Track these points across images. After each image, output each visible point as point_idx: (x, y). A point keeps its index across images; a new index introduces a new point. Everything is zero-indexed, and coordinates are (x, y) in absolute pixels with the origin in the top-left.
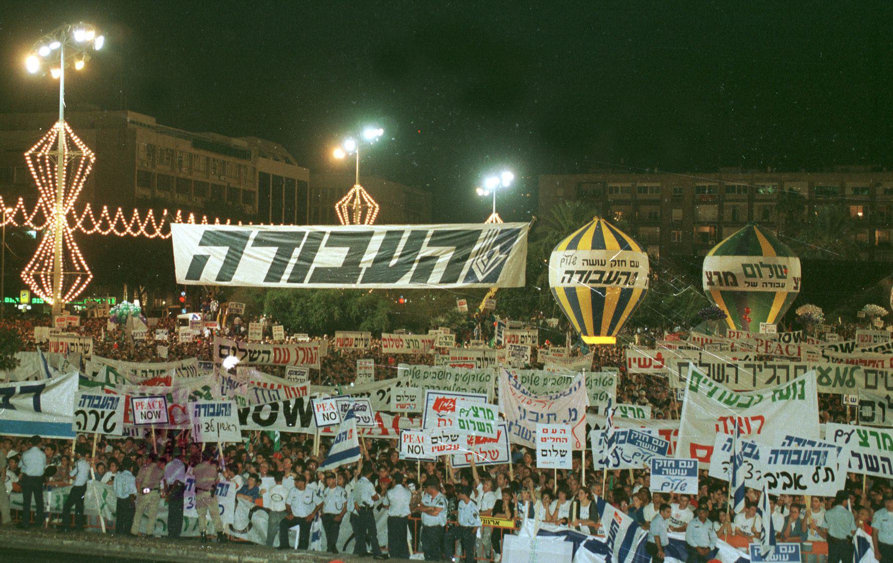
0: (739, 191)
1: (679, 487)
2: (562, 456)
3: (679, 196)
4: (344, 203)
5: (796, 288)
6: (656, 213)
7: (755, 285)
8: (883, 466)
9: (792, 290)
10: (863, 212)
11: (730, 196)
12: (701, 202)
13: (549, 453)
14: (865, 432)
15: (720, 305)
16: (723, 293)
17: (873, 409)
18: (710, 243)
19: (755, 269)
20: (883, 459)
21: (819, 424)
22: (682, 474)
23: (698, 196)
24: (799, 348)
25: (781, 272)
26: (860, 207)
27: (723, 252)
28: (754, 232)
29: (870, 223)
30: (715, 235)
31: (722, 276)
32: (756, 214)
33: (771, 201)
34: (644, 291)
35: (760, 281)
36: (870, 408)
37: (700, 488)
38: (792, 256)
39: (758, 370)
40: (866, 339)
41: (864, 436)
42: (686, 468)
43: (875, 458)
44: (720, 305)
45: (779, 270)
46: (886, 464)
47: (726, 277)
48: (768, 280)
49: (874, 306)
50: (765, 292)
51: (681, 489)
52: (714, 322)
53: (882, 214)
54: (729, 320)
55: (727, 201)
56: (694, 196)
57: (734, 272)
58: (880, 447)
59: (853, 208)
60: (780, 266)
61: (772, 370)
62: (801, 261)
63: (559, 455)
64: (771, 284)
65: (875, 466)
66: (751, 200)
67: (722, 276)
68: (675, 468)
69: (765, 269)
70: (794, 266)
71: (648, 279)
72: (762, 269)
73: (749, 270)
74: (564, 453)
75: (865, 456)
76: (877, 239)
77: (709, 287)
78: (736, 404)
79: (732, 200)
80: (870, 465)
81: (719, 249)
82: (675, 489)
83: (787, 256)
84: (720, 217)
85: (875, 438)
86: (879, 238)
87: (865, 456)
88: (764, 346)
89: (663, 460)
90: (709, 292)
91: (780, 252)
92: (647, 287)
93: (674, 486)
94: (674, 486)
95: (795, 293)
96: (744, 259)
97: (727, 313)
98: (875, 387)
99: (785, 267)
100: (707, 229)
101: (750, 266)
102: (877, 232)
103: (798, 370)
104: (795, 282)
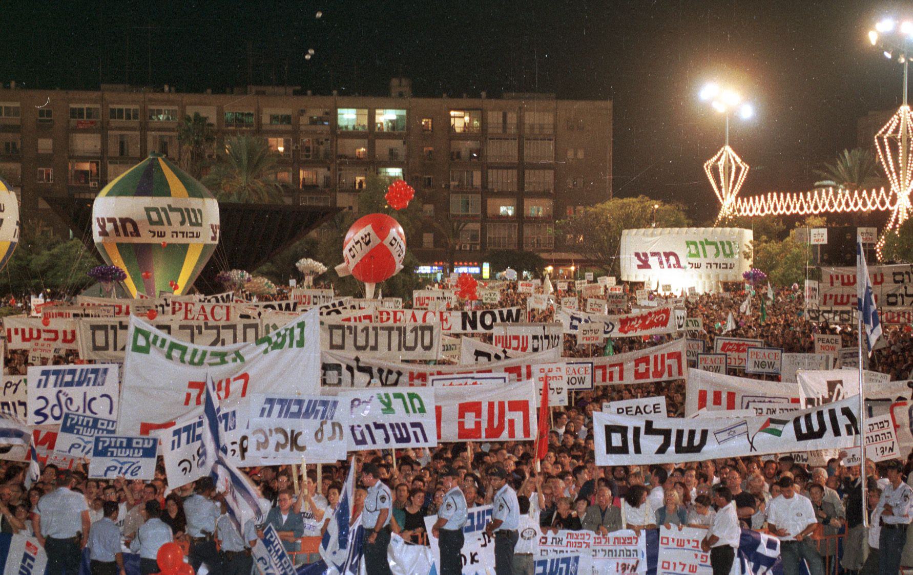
0: (129, 117)
1: (130, 471)
2: (558, 393)
3: (47, 121)
4: (719, 159)
5: (213, 239)
6: (14, 145)
7: (162, 235)
8: (415, 433)
9: (209, 241)
10: (284, 147)
11: (114, 122)
12: (76, 130)
13: (900, 299)
14: (387, 396)
15: (118, 262)
16: (120, 246)
17: (340, 374)
18: (91, 184)
19: (163, 214)
20: (414, 425)
21: (321, 388)
22: (136, 455)
23: (74, 122)
24: (228, 308)
25: (191, 217)
26: (281, 140)
27: (120, 191)
28: (159, 165)
29: (293, 160)
30: (98, 174)
31: (119, 223)
32: (150, 146)
33: (169, 130)
34: (12, 244)
35: (165, 228)
36: (336, 372)
37: (601, 467)
38: (208, 197)
39: (196, 331)
40: (304, 300)
41: (386, 400)
42: (142, 448)
43: (404, 425)
44: (118, 262)
45: (192, 215)
46: (418, 430)
47: (125, 225)
48: (180, 229)
49: (310, 261)
50: (174, 245)
51: (132, 474)
52: (110, 285)
53: (308, 149)
54: (129, 282)
55: (112, 129)
56: (68, 121)
57: (135, 219)
58: (407, 412)
59: (272, 141)
60: (193, 210)
61: (215, 331)
62: (220, 204)
63: (556, 392)
64: (183, 233)
65: (405, 436)
66: (144, 128)
67: (119, 223)
68: (126, 448)
69: (175, 213)
70: (211, 210)
71: (17, 228)
72: (171, 214)
73: (154, 216)
74: (367, 239)
75: (391, 425)
76: (301, 180)
77: (101, 238)
78: (369, 348)
79: (121, 129)
80: (399, 436)
81: (116, 186)
82: (126, 472)
83: (201, 197)
84: (104, 149)
85: (400, 400)
86: (304, 179)
87: (391, 425)
88: (183, 310)
89: (111, 438)
90: (102, 245)
91: (193, 193)
92: (16, 240)
93: (123, 471)
94: (123, 471)
95: (212, 245)
96: (148, 201)
97: (127, 273)
98: (342, 347)
99: (200, 211)
100: (86, 166)
101: (155, 209)
102: (301, 172)
103: (248, 330)
104: (213, 231)
